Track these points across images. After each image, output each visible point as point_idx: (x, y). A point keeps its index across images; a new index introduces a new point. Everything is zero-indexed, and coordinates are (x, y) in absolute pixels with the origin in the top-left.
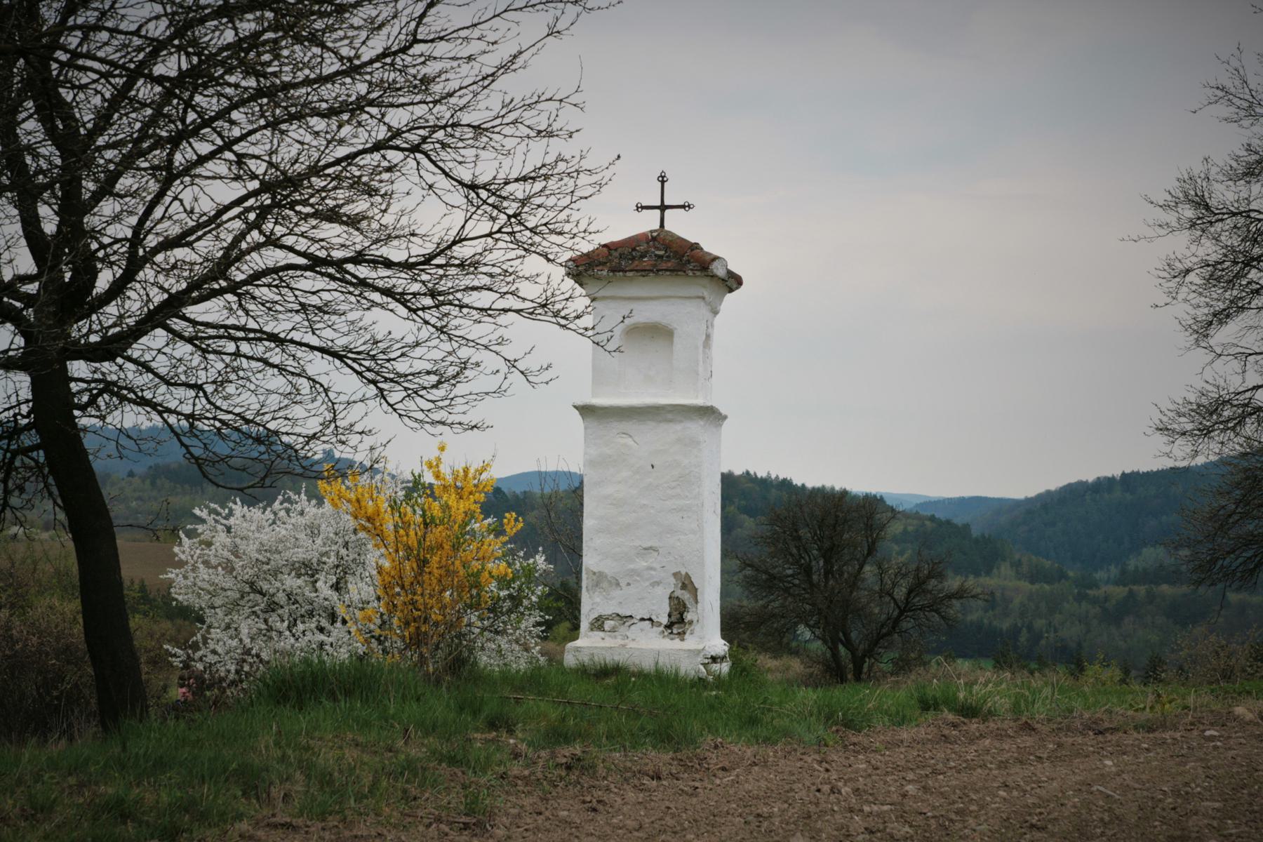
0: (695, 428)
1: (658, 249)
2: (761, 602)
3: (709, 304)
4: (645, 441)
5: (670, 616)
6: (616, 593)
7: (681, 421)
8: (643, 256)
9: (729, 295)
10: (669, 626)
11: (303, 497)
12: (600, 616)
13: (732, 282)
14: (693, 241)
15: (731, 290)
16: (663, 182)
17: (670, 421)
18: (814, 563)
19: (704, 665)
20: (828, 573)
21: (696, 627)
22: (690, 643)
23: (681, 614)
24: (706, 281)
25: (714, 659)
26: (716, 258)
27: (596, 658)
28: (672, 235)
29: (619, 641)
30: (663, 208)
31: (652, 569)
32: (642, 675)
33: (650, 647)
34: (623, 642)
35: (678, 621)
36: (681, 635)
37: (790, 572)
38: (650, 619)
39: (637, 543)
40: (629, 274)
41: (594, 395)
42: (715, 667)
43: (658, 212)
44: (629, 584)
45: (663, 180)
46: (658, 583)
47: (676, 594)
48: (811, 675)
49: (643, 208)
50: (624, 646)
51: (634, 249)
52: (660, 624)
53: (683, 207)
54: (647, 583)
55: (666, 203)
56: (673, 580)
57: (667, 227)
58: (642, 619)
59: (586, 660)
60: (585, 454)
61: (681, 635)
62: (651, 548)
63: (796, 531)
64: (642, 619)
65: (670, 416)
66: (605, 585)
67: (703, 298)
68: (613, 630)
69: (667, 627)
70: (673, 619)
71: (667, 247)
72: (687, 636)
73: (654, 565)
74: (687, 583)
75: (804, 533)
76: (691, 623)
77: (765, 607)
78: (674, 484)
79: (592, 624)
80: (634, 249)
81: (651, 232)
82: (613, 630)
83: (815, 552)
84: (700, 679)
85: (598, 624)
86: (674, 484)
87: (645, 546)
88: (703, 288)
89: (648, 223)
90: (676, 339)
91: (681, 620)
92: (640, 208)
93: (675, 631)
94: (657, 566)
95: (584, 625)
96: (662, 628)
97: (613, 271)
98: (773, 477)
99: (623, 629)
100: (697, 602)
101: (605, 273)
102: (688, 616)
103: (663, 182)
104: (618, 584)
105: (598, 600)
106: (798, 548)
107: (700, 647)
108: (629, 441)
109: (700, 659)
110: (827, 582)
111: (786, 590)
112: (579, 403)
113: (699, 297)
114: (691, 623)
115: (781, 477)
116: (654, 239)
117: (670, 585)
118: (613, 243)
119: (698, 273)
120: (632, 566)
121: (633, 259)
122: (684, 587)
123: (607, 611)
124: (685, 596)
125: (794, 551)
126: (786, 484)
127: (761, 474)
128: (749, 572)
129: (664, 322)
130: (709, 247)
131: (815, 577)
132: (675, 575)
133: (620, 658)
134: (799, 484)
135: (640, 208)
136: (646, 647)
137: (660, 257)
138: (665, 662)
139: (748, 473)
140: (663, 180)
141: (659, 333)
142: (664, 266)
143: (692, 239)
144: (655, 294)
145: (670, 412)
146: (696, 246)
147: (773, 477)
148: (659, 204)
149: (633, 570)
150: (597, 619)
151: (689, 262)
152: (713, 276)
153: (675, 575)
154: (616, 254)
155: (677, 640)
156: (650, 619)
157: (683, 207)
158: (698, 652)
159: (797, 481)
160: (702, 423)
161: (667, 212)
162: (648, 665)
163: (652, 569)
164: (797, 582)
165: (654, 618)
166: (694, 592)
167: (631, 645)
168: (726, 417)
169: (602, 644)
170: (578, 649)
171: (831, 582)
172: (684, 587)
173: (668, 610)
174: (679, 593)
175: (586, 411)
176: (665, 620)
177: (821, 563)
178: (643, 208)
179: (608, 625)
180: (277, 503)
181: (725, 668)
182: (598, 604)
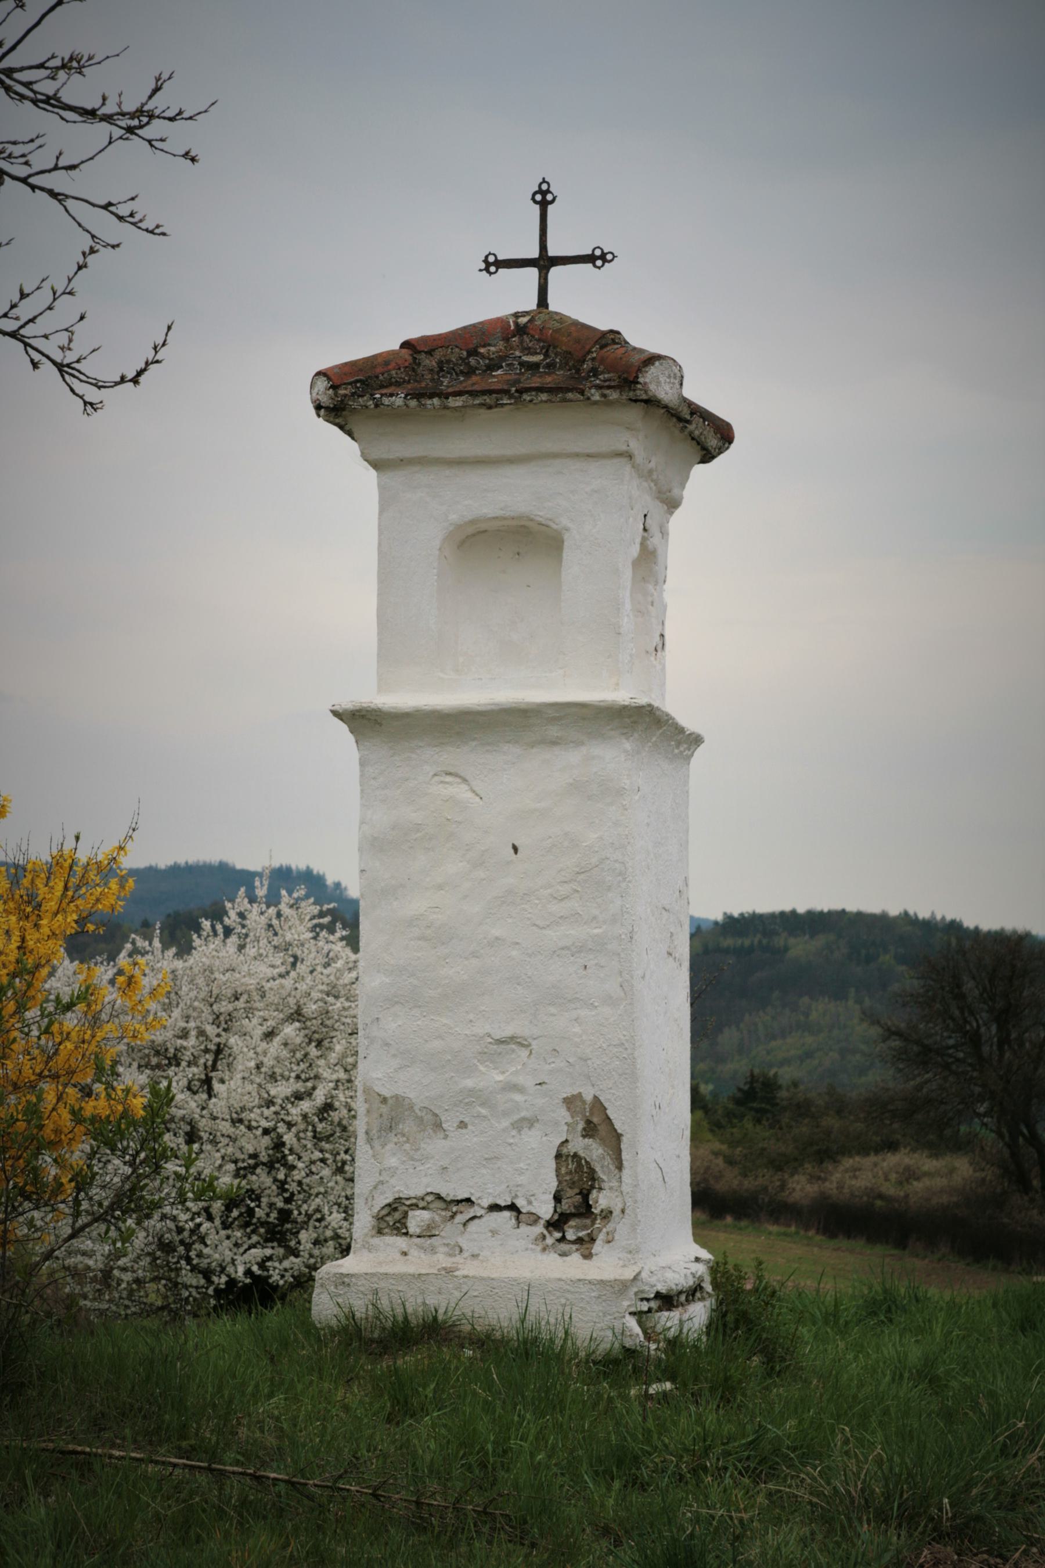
0: (613, 757)
1: (530, 351)
2: (912, 1083)
3: (648, 475)
4: (504, 788)
5: (557, 1198)
6: (435, 1146)
7: (579, 744)
8: (492, 367)
9: (699, 470)
10: (557, 1224)
11: (157, 943)
12: (398, 1200)
13: (705, 436)
14: (604, 327)
15: (707, 457)
16: (544, 205)
17: (554, 743)
18: (983, 1030)
19: (638, 1314)
20: (1004, 1042)
21: (620, 1227)
22: (607, 1264)
23: (585, 1195)
24: (633, 414)
25: (667, 1300)
26: (653, 359)
27: (384, 1304)
28: (561, 318)
29: (442, 1260)
30: (544, 263)
31: (515, 1088)
32: (487, 1343)
33: (513, 1273)
34: (446, 1262)
35: (576, 1211)
36: (585, 1244)
37: (951, 1042)
38: (513, 1207)
39: (482, 1028)
40: (455, 402)
41: (380, 690)
42: (669, 1320)
43: (533, 272)
44: (463, 1125)
45: (543, 199)
46: (531, 1122)
47: (574, 1147)
48: (983, 1180)
49: (500, 264)
50: (449, 1271)
51: (473, 352)
52: (535, 1219)
53: (589, 259)
54: (505, 1123)
55: (552, 252)
56: (563, 1115)
57: (555, 304)
58: (495, 1208)
59: (360, 1306)
60: (362, 822)
61: (585, 1244)
62: (512, 1039)
63: (959, 986)
64: (495, 1208)
65: (554, 731)
66: (408, 1126)
67: (630, 457)
68: (428, 1233)
69: (551, 1225)
70: (566, 1206)
71: (548, 346)
72: (598, 1247)
73: (521, 1080)
74: (596, 1123)
75: (969, 985)
76: (607, 1215)
77: (919, 1088)
78: (564, 890)
79: (380, 1219)
80: (473, 352)
81: (517, 315)
82: (428, 1233)
83: (985, 1015)
84: (630, 1353)
85: (394, 1218)
86: (564, 890)
87: (499, 1034)
88: (630, 433)
89: (513, 296)
90: (567, 554)
91: (585, 1210)
92: (493, 264)
93: (571, 1235)
94: (527, 1081)
95: (363, 1221)
96: (539, 1229)
97: (418, 396)
98: (939, 917)
99: (449, 1232)
100: (620, 1167)
101: (398, 401)
102: (601, 1200)
103: (544, 205)
104: (438, 1126)
105: (393, 1162)
106: (962, 1010)
107: (629, 1274)
108: (462, 792)
109: (627, 1303)
110: (1001, 1056)
111: (947, 1066)
112: (348, 701)
113: (620, 454)
114: (607, 1215)
115: (948, 918)
116: (521, 330)
117: (558, 1128)
118: (425, 339)
119: (614, 395)
120: (469, 1083)
121: (470, 372)
122: (590, 1130)
123: (414, 1187)
124: (593, 1151)
125: (957, 1013)
126: (954, 927)
127: (924, 914)
128: (896, 1043)
129: (541, 513)
130: (641, 338)
131: (986, 1049)
132: (570, 1102)
133: (440, 1300)
134: (972, 926)
135: (493, 264)
136: (505, 1274)
137: (534, 367)
138: (546, 1314)
139: (906, 913)
140: (543, 199)
141: (528, 541)
142: (536, 382)
143: (602, 323)
144: (522, 450)
145: (554, 720)
146: (612, 338)
147: (939, 917)
148: (535, 254)
149: (471, 1091)
150: (392, 1207)
151: (595, 372)
152: (651, 403)
153: (570, 1102)
154: (430, 362)
155: (576, 1257)
156: (513, 1207)
157: (589, 259)
158: (622, 1287)
159: (969, 923)
160: (628, 746)
161: (555, 272)
162: (500, 1315)
163: (515, 1088)
164: (961, 1055)
165: (520, 1203)
166: (614, 1140)
167: (468, 1269)
168: (696, 740)
169: (402, 1267)
170: (343, 1280)
171: (1007, 1055)
172: (590, 1130)
173: (553, 1185)
174: (579, 1145)
175: (362, 721)
176: (546, 1210)
177: (994, 1029)
178: (500, 264)
179: (417, 1220)
180: (123, 954)
181: (697, 1315)
182: (393, 1171)
